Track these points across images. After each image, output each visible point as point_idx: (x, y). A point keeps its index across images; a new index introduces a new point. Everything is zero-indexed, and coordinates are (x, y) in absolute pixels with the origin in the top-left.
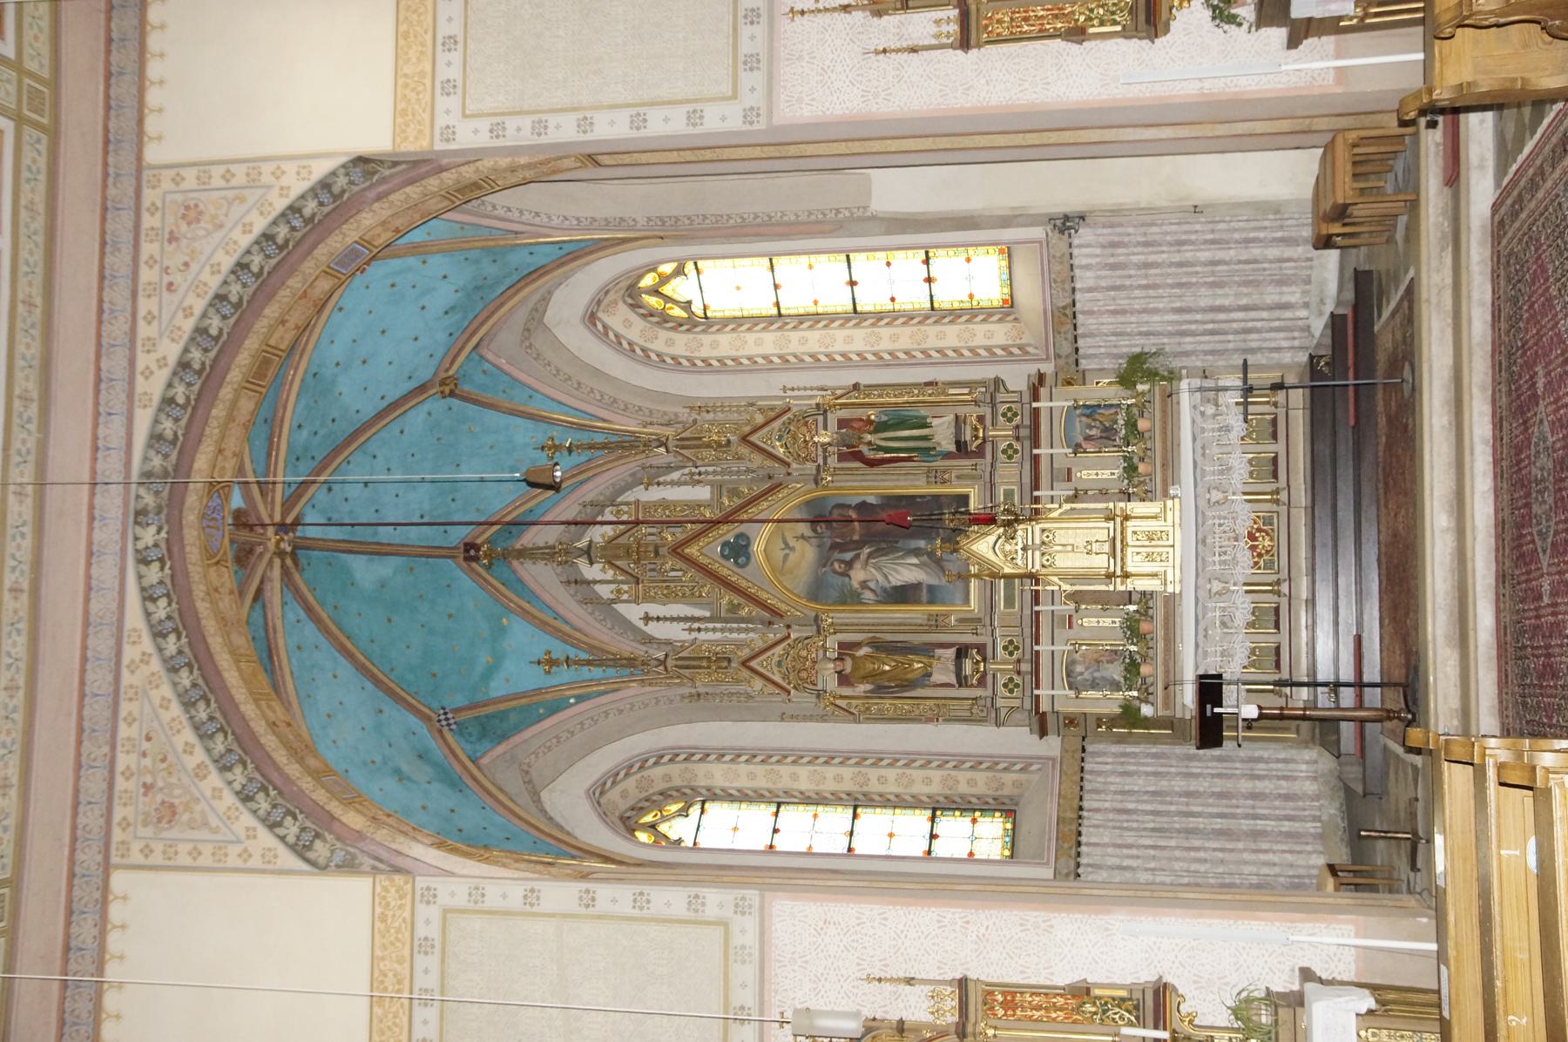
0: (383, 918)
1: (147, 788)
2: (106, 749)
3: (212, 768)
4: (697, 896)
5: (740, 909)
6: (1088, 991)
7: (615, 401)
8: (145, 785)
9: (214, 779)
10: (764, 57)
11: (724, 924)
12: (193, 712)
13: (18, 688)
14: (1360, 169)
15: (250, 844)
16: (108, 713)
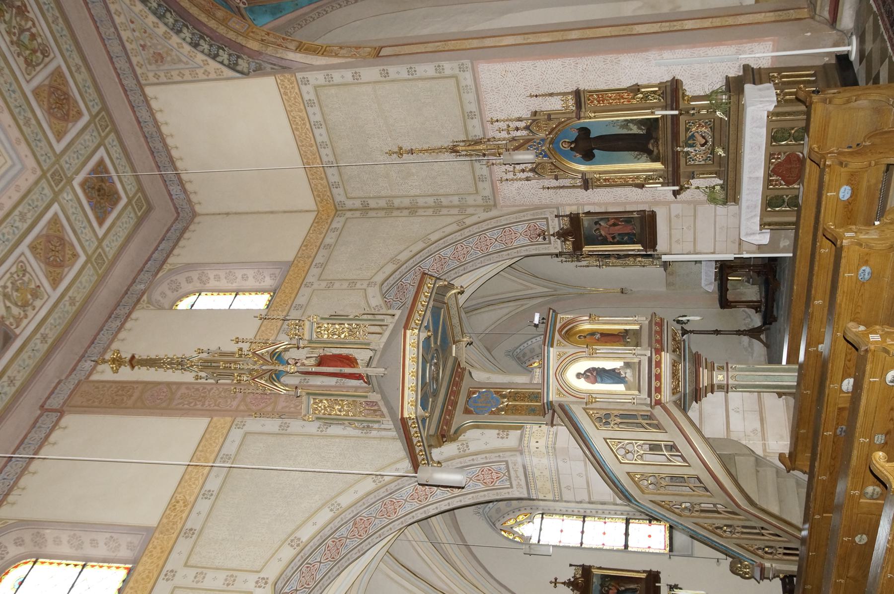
0: (286, 94)
1: (143, 47)
2: (113, 30)
3: (172, 33)
4: (439, 66)
5: (462, 69)
6: (639, 90)
8: (141, 45)
9: (175, 39)
11: (455, 77)
12: (149, 5)
13: (58, 18)
15: (206, 67)
16: (105, 11)
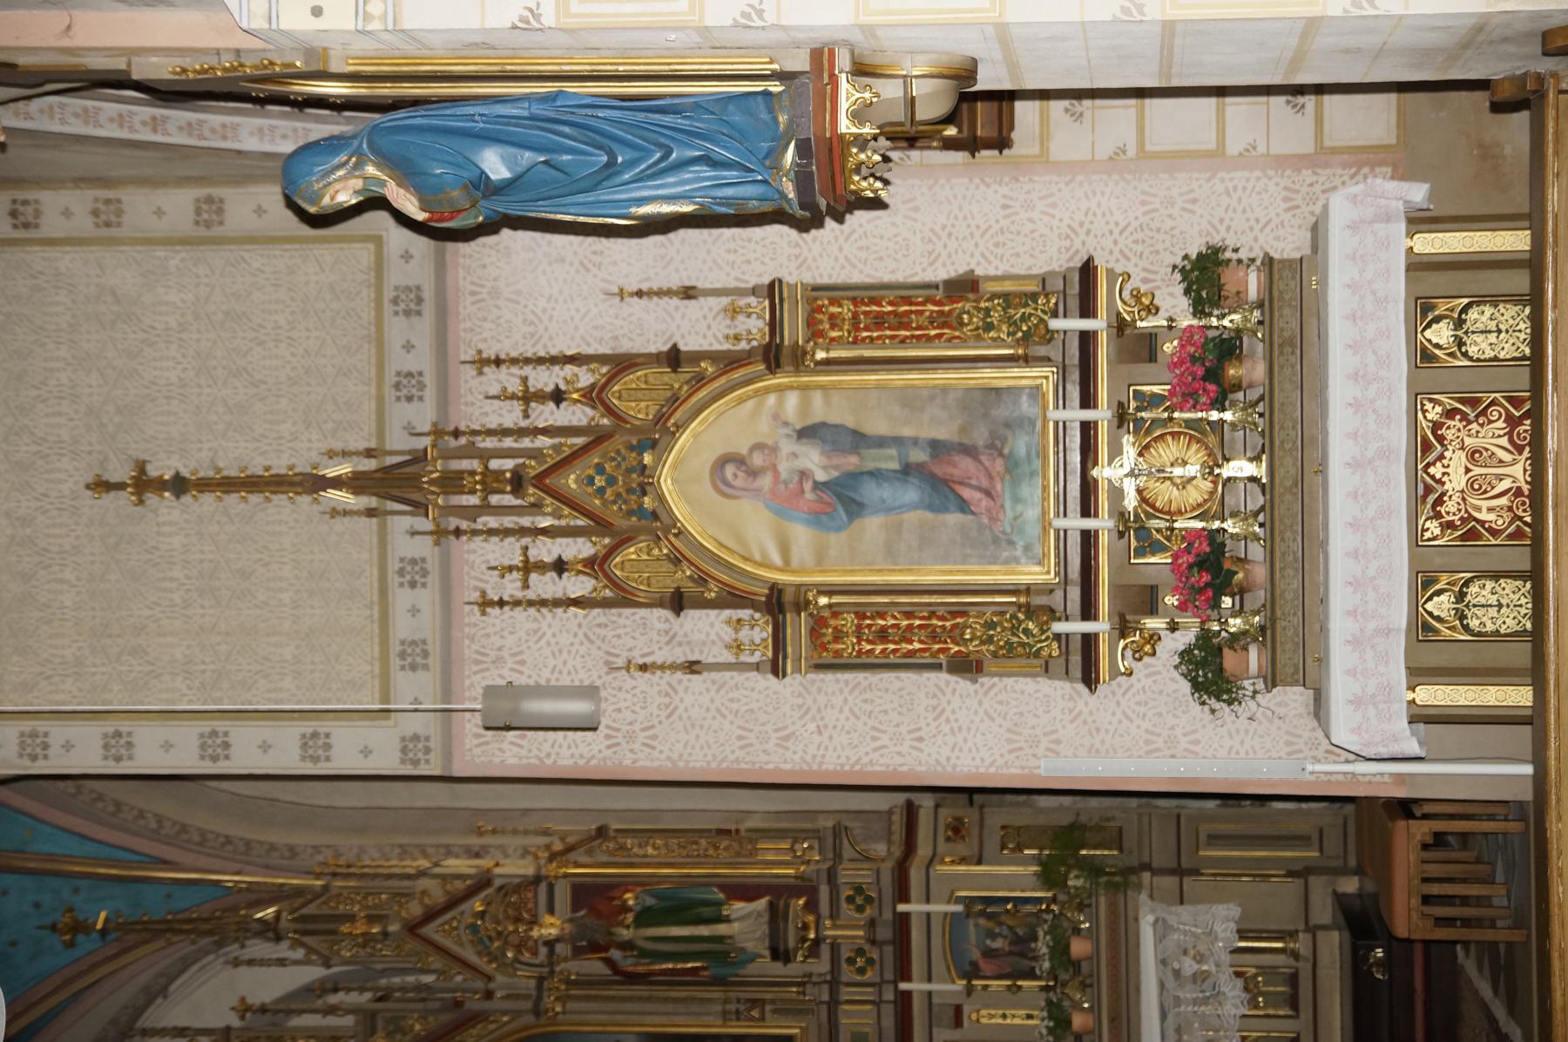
7: (184, 828)
10: (434, 647)
14: (1436, 889)
